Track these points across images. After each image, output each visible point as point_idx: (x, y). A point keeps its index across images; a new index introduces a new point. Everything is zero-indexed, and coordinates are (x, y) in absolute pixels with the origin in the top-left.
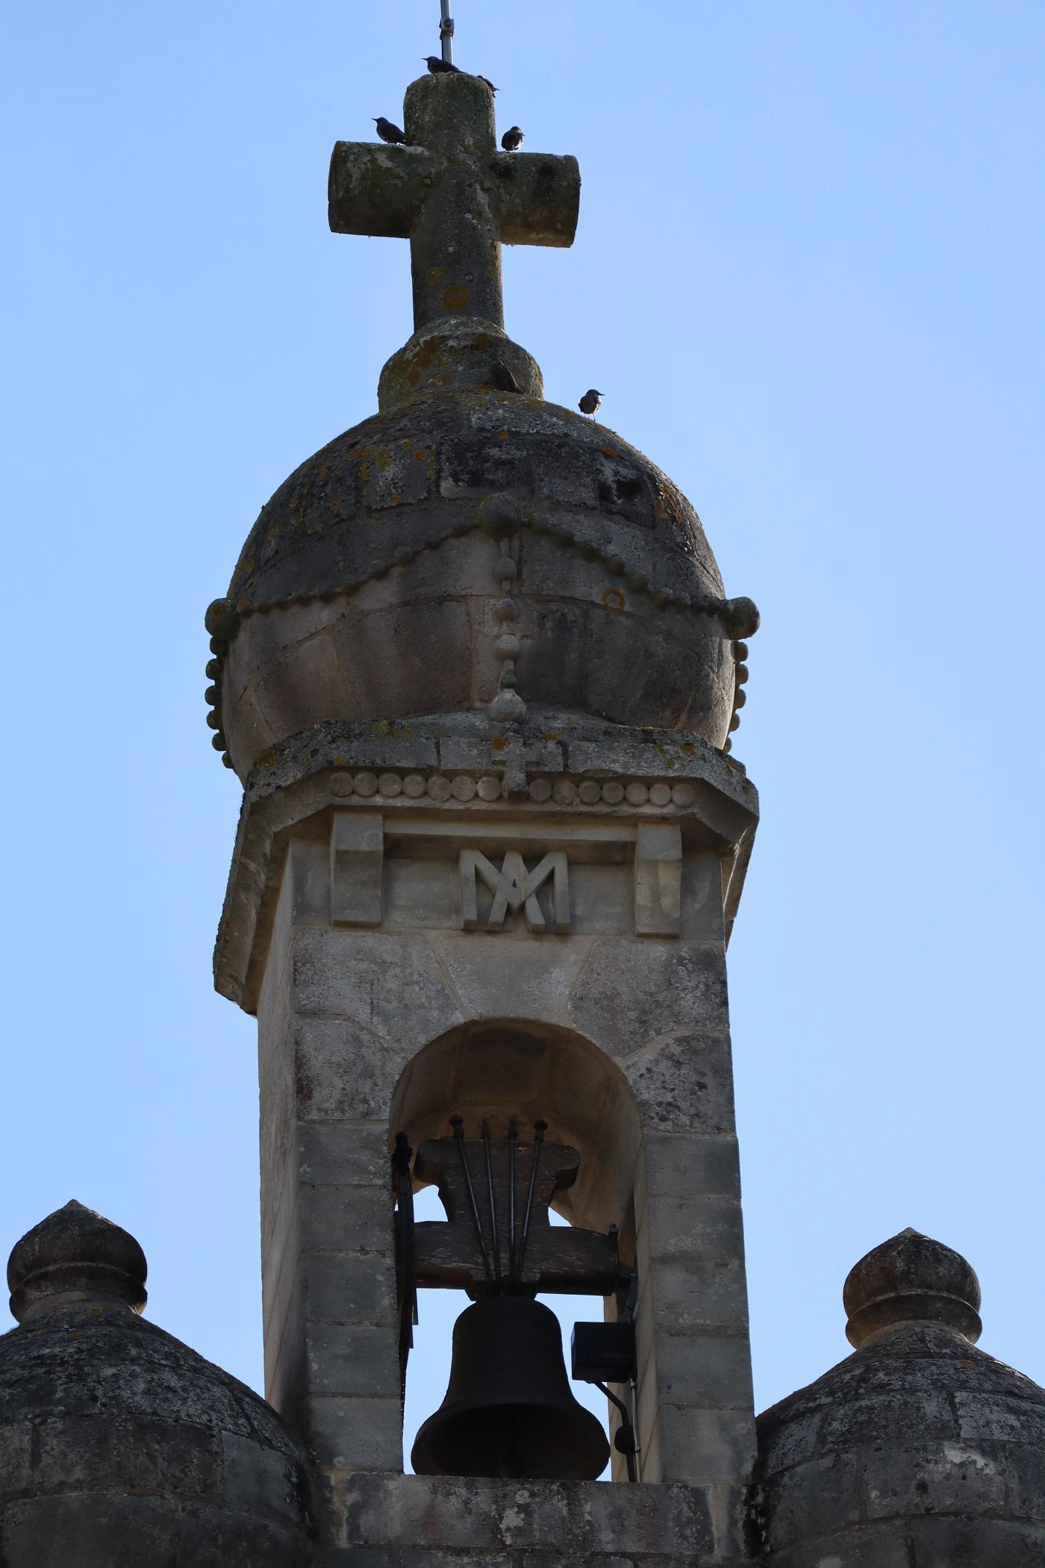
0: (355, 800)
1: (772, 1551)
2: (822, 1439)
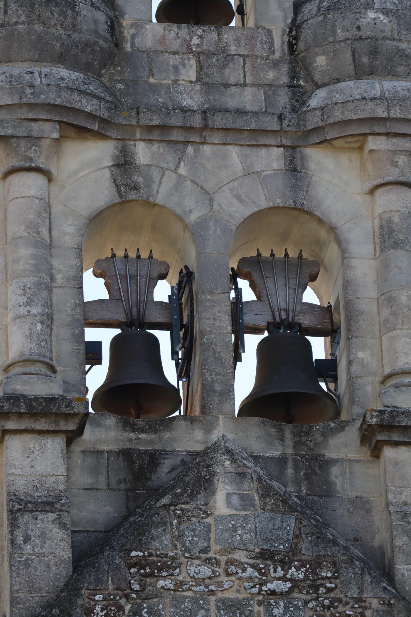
1: (298, 54)
2: (319, 9)
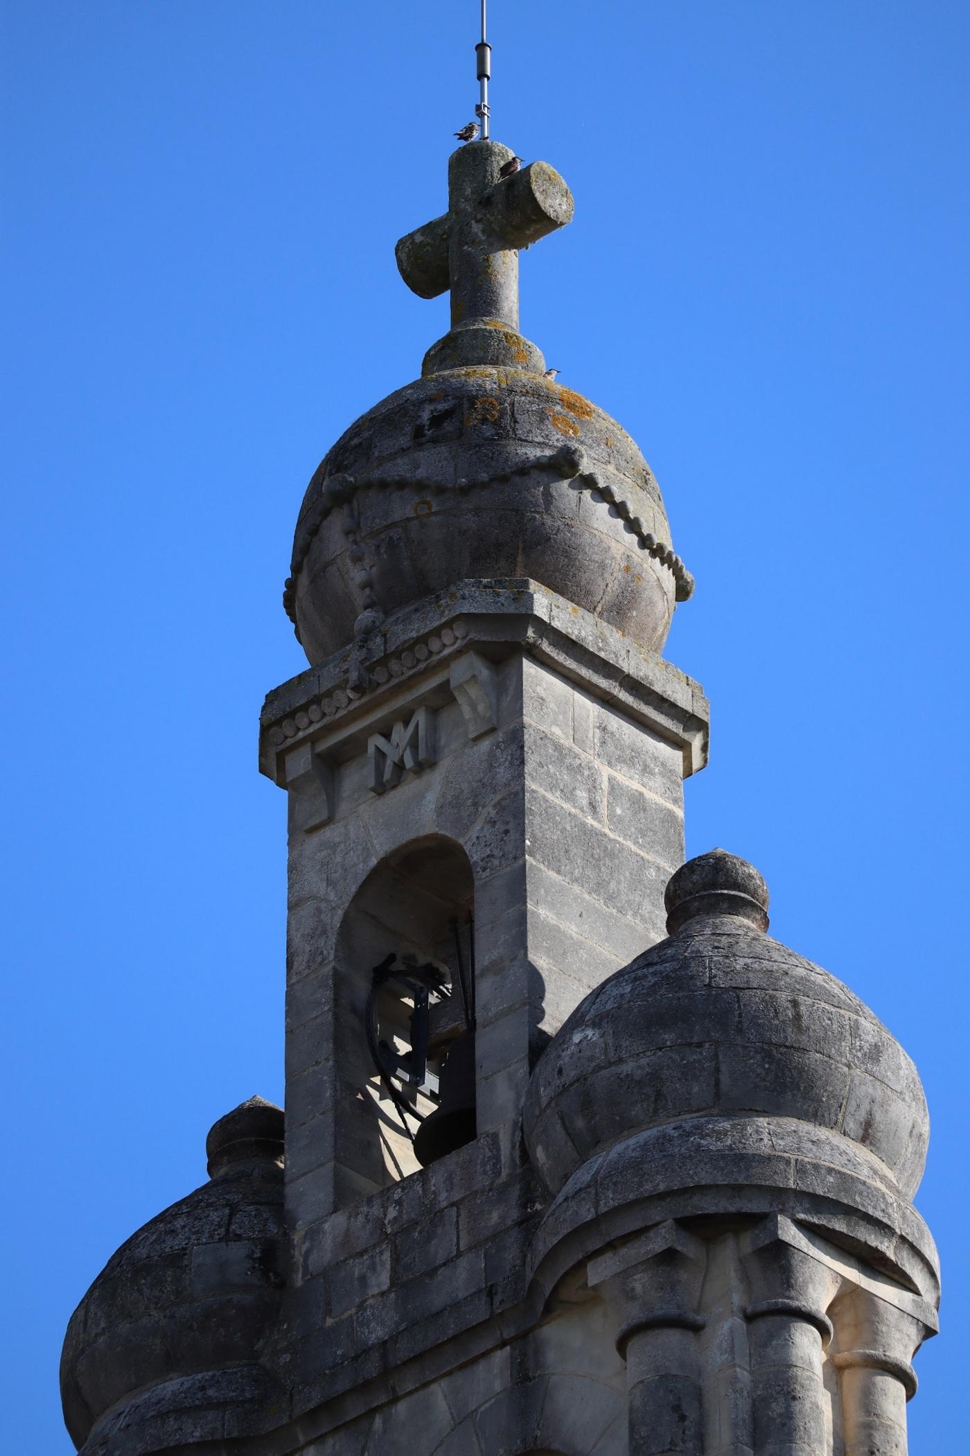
0: (290, 741)
